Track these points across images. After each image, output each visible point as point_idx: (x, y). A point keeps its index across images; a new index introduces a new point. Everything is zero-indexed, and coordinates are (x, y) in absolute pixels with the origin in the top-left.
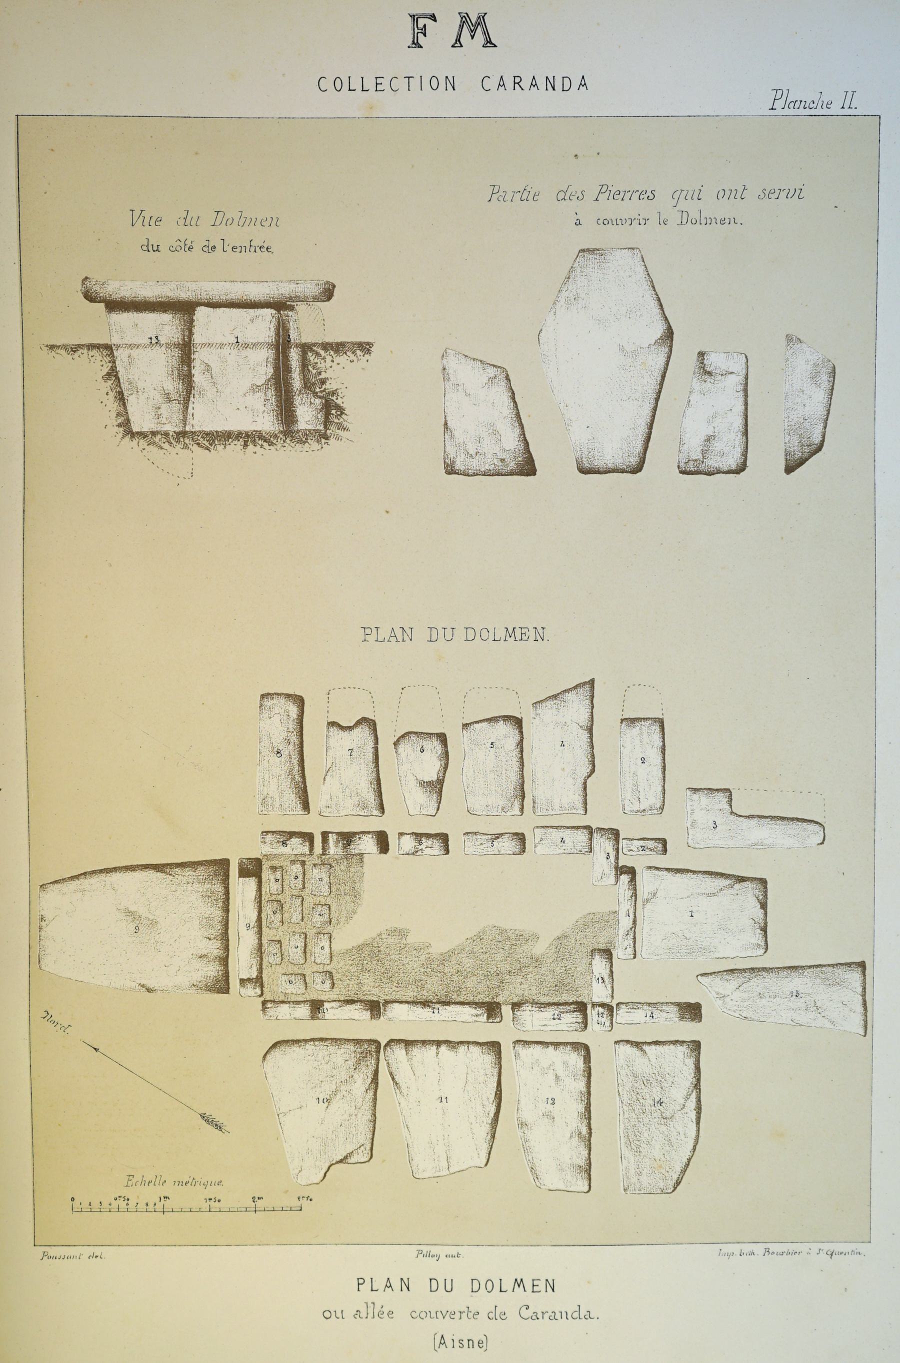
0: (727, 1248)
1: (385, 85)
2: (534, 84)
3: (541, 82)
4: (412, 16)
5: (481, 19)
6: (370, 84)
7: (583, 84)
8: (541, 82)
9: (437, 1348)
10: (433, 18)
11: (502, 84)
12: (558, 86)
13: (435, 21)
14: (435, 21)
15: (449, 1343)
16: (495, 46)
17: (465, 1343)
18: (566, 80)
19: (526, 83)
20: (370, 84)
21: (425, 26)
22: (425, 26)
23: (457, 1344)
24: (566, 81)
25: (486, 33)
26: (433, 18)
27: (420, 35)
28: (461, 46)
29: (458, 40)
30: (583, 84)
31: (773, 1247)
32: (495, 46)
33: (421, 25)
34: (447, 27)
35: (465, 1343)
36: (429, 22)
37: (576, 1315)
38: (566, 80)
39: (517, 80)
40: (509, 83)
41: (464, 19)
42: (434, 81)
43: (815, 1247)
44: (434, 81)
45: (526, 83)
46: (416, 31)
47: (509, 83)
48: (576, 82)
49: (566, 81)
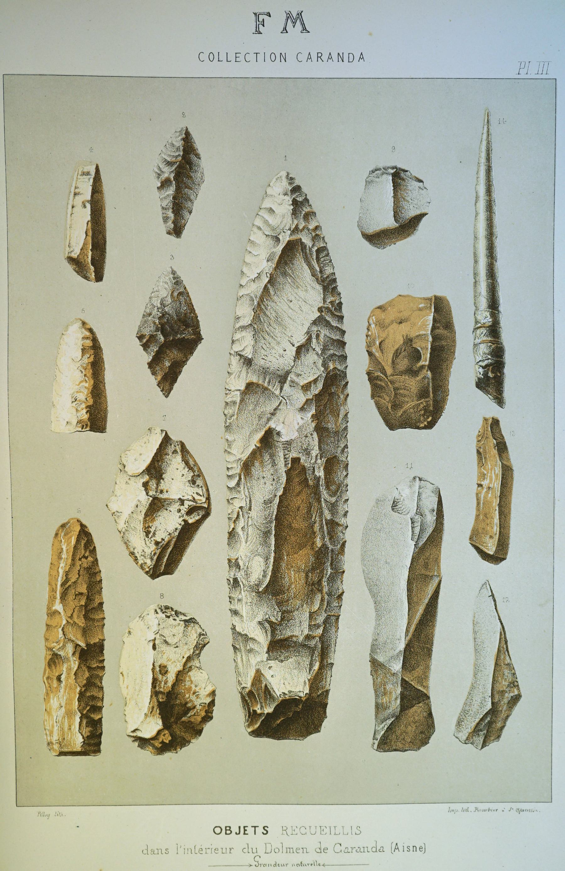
0: (453, 806)
1: (241, 58)
2: (330, 57)
3: (335, 56)
4: (255, 14)
5: (300, 14)
6: (232, 57)
7: (362, 57)
8: (335, 56)
9: (393, 852)
10: (269, 15)
11: (309, 57)
12: (346, 59)
13: (270, 16)
14: (270, 16)
15: (401, 849)
16: (309, 32)
17: (411, 848)
18: (351, 55)
19: (325, 57)
20: (232, 57)
21: (263, 20)
22: (263, 20)
23: (406, 849)
24: (351, 56)
25: (303, 24)
26: (269, 15)
27: (261, 26)
28: (287, 32)
29: (285, 29)
30: (362, 57)
31: (481, 806)
32: (309, 32)
33: (261, 20)
34: (278, 20)
35: (411, 848)
36: (266, 17)
37: (374, 849)
38: (351, 55)
39: (320, 55)
40: (314, 57)
41: (289, 16)
42: (273, 55)
43: (508, 806)
44: (273, 55)
45: (325, 57)
46: (258, 23)
47: (314, 57)
48: (357, 57)
49: (351, 56)
